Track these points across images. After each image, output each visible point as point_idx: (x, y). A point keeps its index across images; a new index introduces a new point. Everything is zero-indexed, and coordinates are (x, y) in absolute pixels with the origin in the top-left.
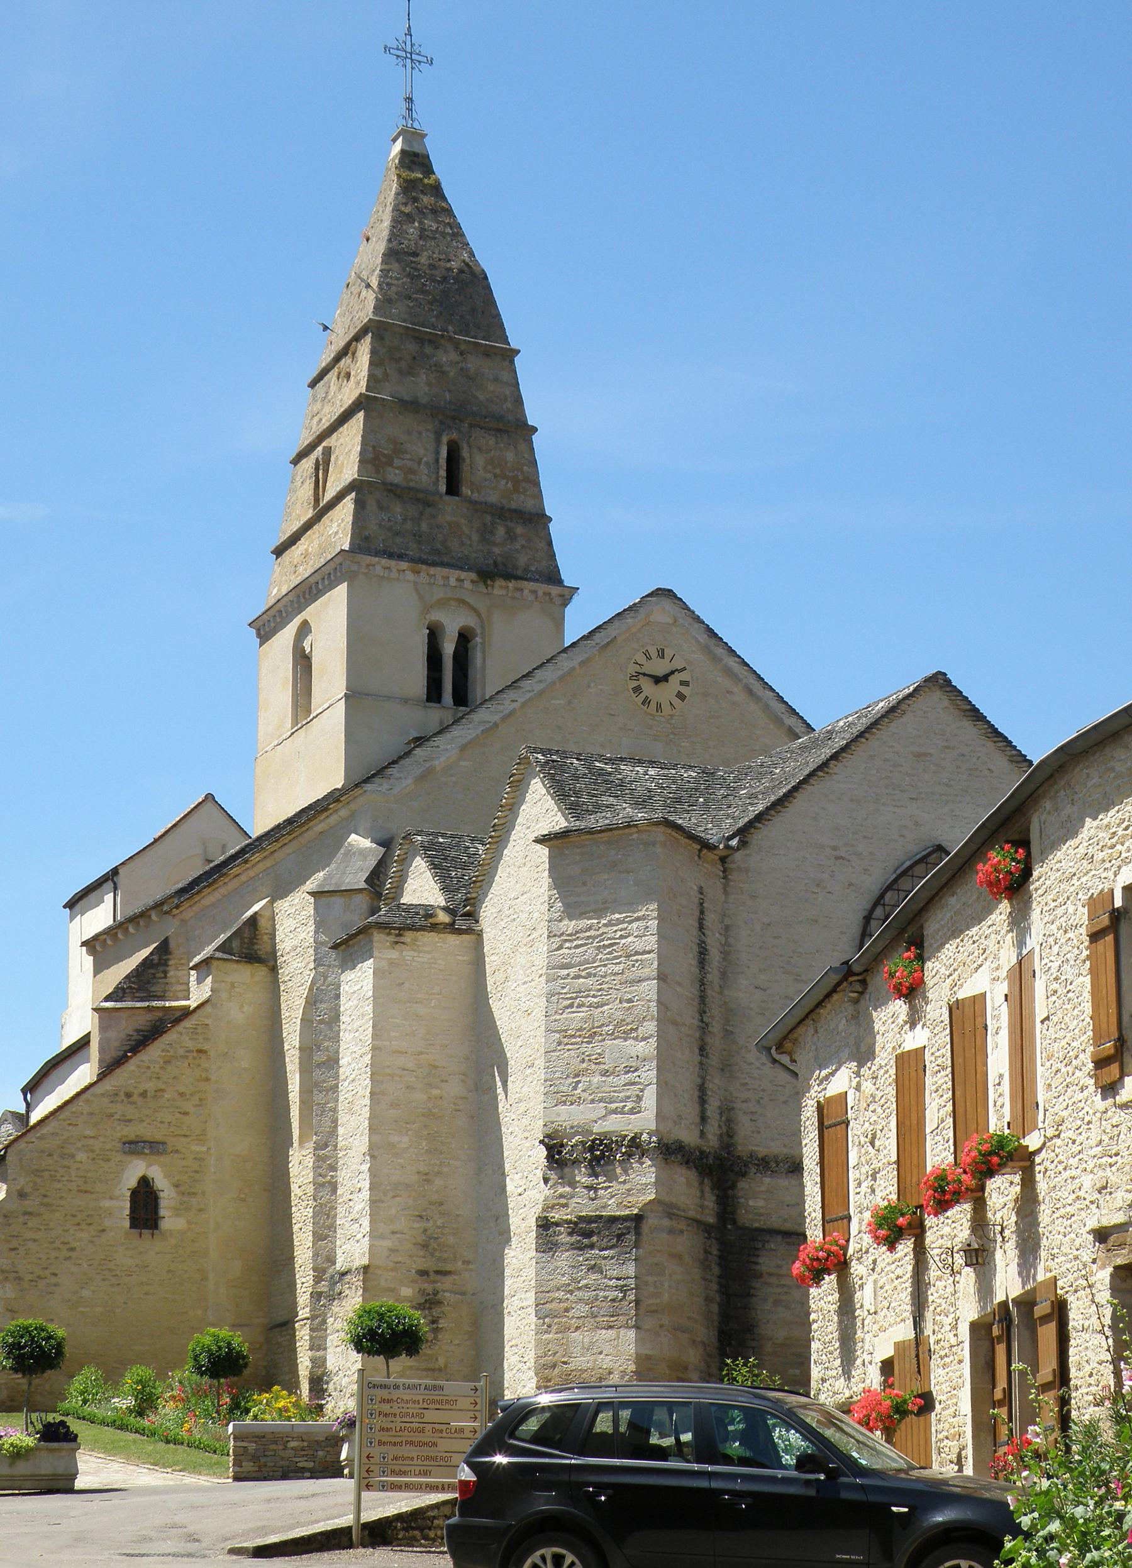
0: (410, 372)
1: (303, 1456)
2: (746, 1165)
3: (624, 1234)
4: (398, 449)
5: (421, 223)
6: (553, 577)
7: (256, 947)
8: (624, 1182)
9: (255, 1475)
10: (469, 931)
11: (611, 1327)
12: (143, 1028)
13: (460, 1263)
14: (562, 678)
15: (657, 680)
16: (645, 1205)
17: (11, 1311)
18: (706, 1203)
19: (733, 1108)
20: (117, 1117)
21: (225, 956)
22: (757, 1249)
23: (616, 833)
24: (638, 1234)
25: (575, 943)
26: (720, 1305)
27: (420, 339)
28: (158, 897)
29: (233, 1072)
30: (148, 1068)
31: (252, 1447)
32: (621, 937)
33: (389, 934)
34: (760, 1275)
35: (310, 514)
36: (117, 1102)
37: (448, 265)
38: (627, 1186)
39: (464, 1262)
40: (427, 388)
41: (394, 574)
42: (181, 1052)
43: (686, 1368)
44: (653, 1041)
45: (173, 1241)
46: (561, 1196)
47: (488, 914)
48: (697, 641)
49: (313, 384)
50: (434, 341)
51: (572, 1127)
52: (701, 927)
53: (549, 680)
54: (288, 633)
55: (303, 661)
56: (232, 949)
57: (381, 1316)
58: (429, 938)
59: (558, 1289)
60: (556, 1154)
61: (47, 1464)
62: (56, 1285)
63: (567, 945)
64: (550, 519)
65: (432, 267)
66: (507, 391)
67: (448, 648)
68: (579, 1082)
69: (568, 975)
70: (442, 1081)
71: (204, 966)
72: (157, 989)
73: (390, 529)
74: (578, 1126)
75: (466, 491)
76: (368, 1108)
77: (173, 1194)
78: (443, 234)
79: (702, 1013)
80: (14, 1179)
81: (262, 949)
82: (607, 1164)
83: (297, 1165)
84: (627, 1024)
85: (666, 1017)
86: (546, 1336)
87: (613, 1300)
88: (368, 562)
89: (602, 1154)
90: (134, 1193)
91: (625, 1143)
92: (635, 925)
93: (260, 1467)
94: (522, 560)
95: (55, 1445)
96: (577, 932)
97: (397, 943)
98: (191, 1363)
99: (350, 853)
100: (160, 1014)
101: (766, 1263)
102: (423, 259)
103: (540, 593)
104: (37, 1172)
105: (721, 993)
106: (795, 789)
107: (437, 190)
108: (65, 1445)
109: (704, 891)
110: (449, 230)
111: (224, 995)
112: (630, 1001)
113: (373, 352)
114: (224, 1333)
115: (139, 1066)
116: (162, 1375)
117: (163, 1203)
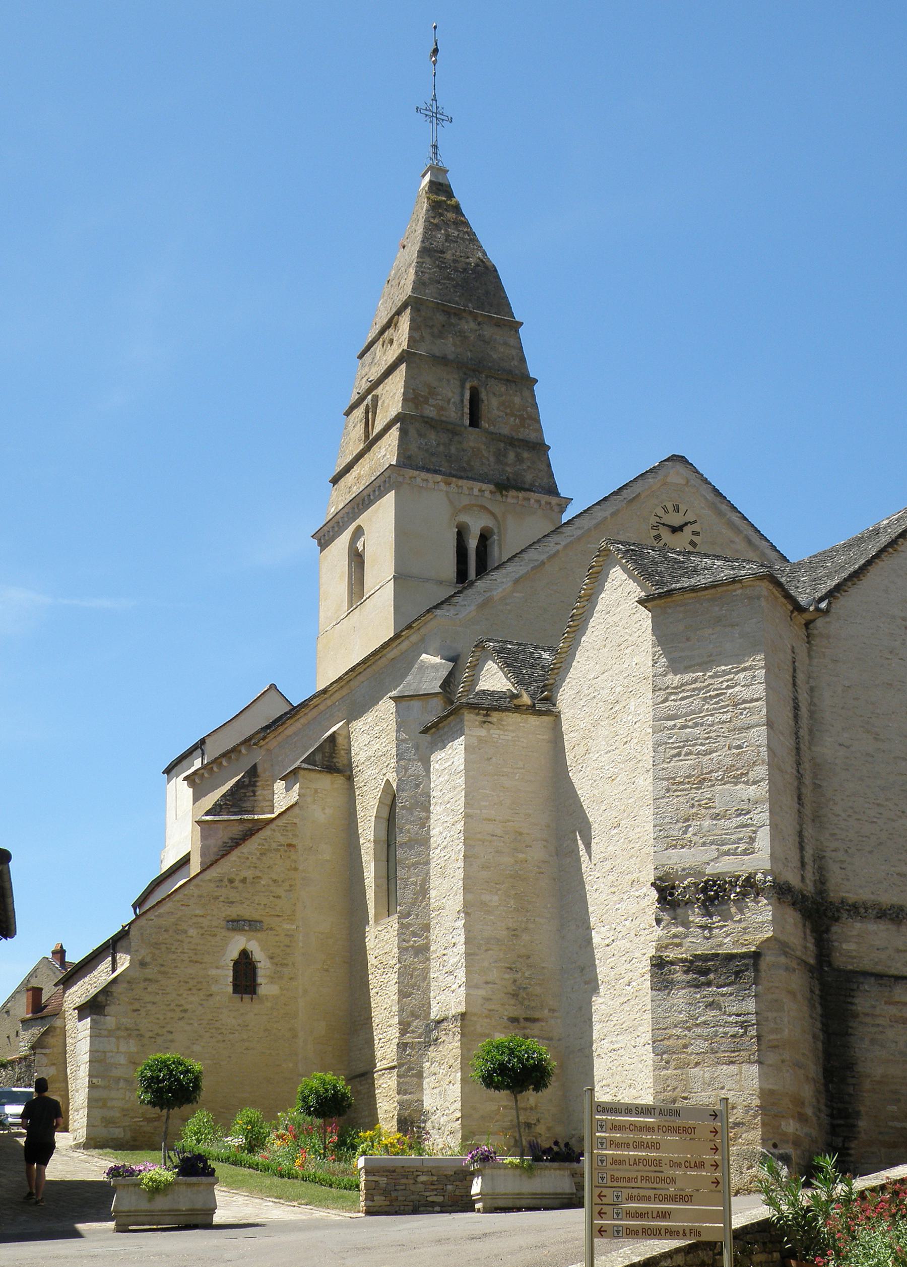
0: (441, 335)
1: (433, 1190)
2: (838, 911)
3: (743, 971)
4: (432, 392)
5: (446, 230)
6: (552, 490)
7: (335, 760)
8: (740, 921)
9: (386, 1209)
10: (548, 713)
11: (732, 1063)
12: (237, 837)
13: (546, 1011)
14: (597, 526)
15: (675, 530)
16: (763, 942)
17: (134, 1063)
18: (808, 945)
19: (824, 857)
20: (221, 899)
21: (310, 767)
22: (853, 990)
23: (719, 589)
24: (757, 970)
25: (681, 695)
26: (823, 1043)
27: (447, 312)
28: (248, 734)
29: (318, 863)
30: (248, 858)
31: (383, 1181)
32: (728, 687)
33: (478, 714)
34: (855, 1016)
35: (362, 446)
36: (221, 886)
37: (467, 260)
38: (743, 925)
39: (550, 1010)
40: (453, 349)
41: (431, 485)
42: (274, 845)
43: (803, 1103)
44: (765, 785)
45: (269, 1004)
46: (675, 936)
47: (566, 696)
48: (706, 499)
49: (361, 356)
50: (458, 314)
51: (684, 870)
52: (794, 684)
53: (586, 528)
54: (345, 538)
55: (357, 559)
56: (315, 761)
57: (512, 1052)
58: (513, 718)
59: (676, 1026)
60: (668, 895)
61: (185, 1199)
62: (172, 1041)
63: (673, 697)
64: (549, 448)
65: (455, 261)
66: (514, 352)
67: (473, 544)
68: (690, 826)
69: (675, 725)
70: (527, 846)
71: (290, 777)
72: (247, 805)
73: (427, 451)
74: (690, 868)
75: (484, 424)
76: (462, 870)
77: (269, 965)
78: (463, 239)
79: (798, 764)
80: (137, 951)
81: (340, 761)
82: (721, 904)
83: (373, 940)
84: (737, 769)
85: (774, 766)
86: (664, 1072)
87: (733, 1036)
88: (411, 474)
89: (715, 895)
90: (236, 963)
91: (740, 883)
92: (742, 675)
93: (391, 1201)
94: (529, 477)
95: (194, 1179)
96: (682, 685)
97: (485, 722)
98: (300, 1104)
99: (423, 667)
100: (250, 826)
101: (862, 1004)
102: (448, 256)
103: (543, 502)
104: (156, 945)
105: (810, 749)
106: (869, 563)
107: (457, 209)
108: (204, 1179)
109: (796, 651)
110: (466, 237)
111: (309, 800)
112: (739, 747)
113: (412, 320)
114: (329, 1077)
115: (239, 857)
116: (270, 1115)
117: (260, 972)
